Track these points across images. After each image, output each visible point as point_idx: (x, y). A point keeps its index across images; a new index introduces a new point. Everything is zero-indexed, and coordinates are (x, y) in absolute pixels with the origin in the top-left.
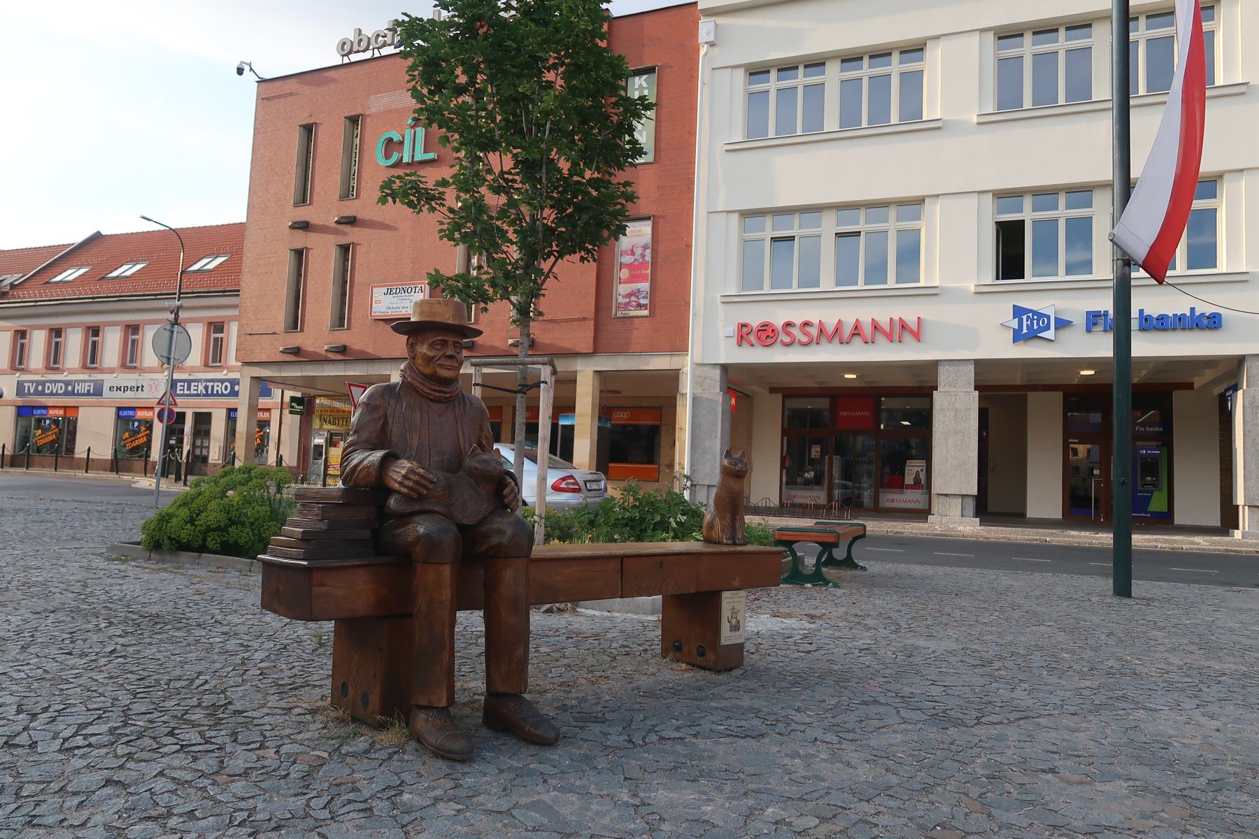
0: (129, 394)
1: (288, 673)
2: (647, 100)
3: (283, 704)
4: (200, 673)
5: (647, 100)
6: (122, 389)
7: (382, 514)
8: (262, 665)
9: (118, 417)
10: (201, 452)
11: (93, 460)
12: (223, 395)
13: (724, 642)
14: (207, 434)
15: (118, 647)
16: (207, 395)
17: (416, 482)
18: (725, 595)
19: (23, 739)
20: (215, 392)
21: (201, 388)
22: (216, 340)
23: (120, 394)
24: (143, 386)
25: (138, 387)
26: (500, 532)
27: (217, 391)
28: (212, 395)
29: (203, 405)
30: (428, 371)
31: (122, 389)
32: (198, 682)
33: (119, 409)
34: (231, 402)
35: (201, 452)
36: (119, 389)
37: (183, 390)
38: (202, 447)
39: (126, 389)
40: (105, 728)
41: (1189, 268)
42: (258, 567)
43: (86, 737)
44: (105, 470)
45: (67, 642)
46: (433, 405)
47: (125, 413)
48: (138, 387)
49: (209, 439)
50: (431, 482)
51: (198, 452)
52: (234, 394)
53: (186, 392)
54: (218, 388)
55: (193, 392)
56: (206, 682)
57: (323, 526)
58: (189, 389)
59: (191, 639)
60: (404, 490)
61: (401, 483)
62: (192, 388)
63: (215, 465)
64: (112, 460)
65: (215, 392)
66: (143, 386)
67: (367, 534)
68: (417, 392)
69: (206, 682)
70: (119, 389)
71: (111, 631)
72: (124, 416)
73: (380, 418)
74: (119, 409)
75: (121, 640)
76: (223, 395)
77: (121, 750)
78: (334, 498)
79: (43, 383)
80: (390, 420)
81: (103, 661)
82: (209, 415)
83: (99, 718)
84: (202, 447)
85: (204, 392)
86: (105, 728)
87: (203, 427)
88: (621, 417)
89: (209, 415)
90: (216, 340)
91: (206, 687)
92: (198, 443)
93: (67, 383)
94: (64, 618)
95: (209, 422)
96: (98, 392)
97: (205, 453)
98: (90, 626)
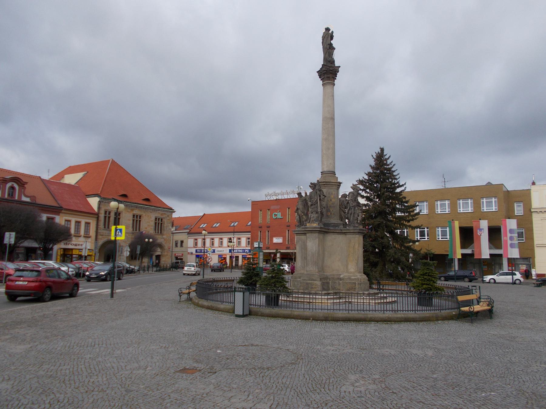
0: (221, 252)
2: (396, 179)
5: (396, 179)
9: (219, 257)
14: (238, 260)
16: (238, 252)
21: (236, 251)
22: (239, 241)
23: (219, 252)
28: (239, 252)
29: (236, 254)
33: (219, 255)
39: (220, 251)
41: (55, 217)
47: (244, 256)
54: (240, 251)
72: (220, 256)
74: (219, 255)
79: (245, 250)
88: (43, 258)
89: (238, 256)
90: (239, 241)
93: (243, 250)
95: (238, 258)
96: (214, 251)
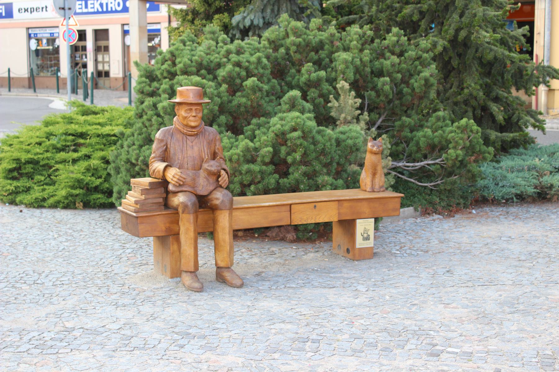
1: (140, 259)
3: (135, 272)
4: (101, 259)
6: (29, 10)
7: (167, 192)
8: (130, 255)
10: (103, 67)
11: (13, 78)
12: (116, 11)
13: (358, 246)
15: (66, 247)
16: (103, 12)
17: (178, 179)
18: (358, 221)
19: (39, 282)
20: (109, 9)
23: (27, 15)
24: (46, 7)
25: (42, 8)
26: (217, 199)
27: (111, 8)
28: (107, 12)
30: (185, 123)
31: (29, 10)
32: (101, 263)
34: (123, 16)
35: (103, 67)
36: (26, 10)
37: (81, 8)
38: (103, 62)
39: (32, 10)
40: (66, 279)
42: (119, 216)
43: (61, 281)
44: (24, 87)
45: (42, 244)
46: (188, 137)
48: (42, 8)
49: (109, 54)
50: (184, 179)
51: (100, 68)
52: (125, 10)
53: (85, 10)
55: (91, 10)
56: (104, 263)
57: (143, 197)
58: (86, 7)
59: (98, 243)
60: (173, 182)
61: (172, 179)
62: (90, 6)
63: (116, 79)
64: (29, 78)
65: (109, 9)
66: (46, 7)
67: (161, 200)
68: (181, 132)
69: (104, 263)
70: (26, 10)
71: (60, 239)
73: (164, 146)
75: (66, 244)
76: (116, 11)
77: (74, 285)
78: (145, 186)
80: (169, 146)
81: (60, 253)
82: (106, 31)
83: (64, 275)
84: (103, 62)
85: (100, 10)
86: (66, 279)
87: (102, 43)
91: (104, 265)
92: (100, 58)
94: (37, 233)
97: (106, 68)
98: (50, 237)
